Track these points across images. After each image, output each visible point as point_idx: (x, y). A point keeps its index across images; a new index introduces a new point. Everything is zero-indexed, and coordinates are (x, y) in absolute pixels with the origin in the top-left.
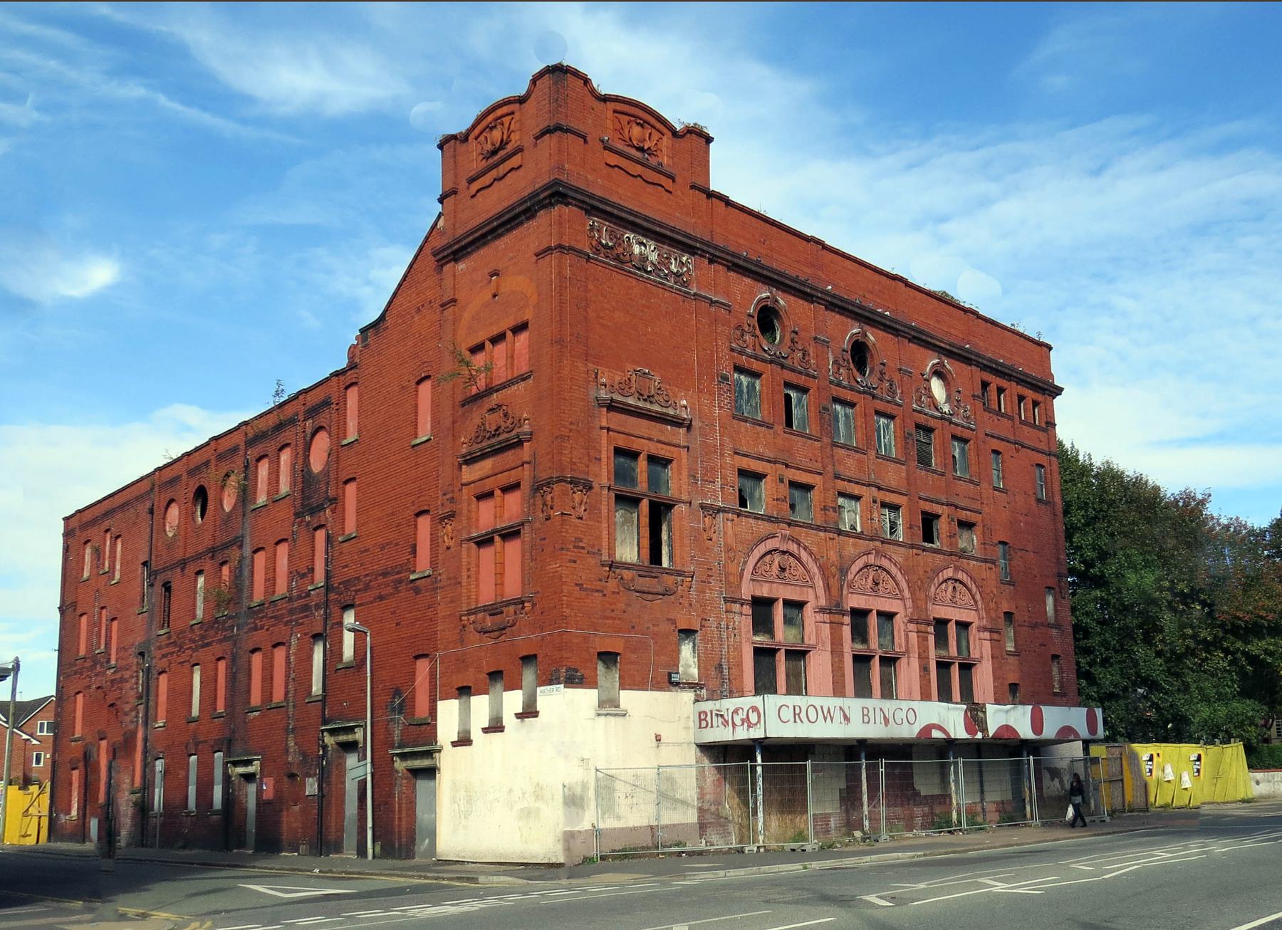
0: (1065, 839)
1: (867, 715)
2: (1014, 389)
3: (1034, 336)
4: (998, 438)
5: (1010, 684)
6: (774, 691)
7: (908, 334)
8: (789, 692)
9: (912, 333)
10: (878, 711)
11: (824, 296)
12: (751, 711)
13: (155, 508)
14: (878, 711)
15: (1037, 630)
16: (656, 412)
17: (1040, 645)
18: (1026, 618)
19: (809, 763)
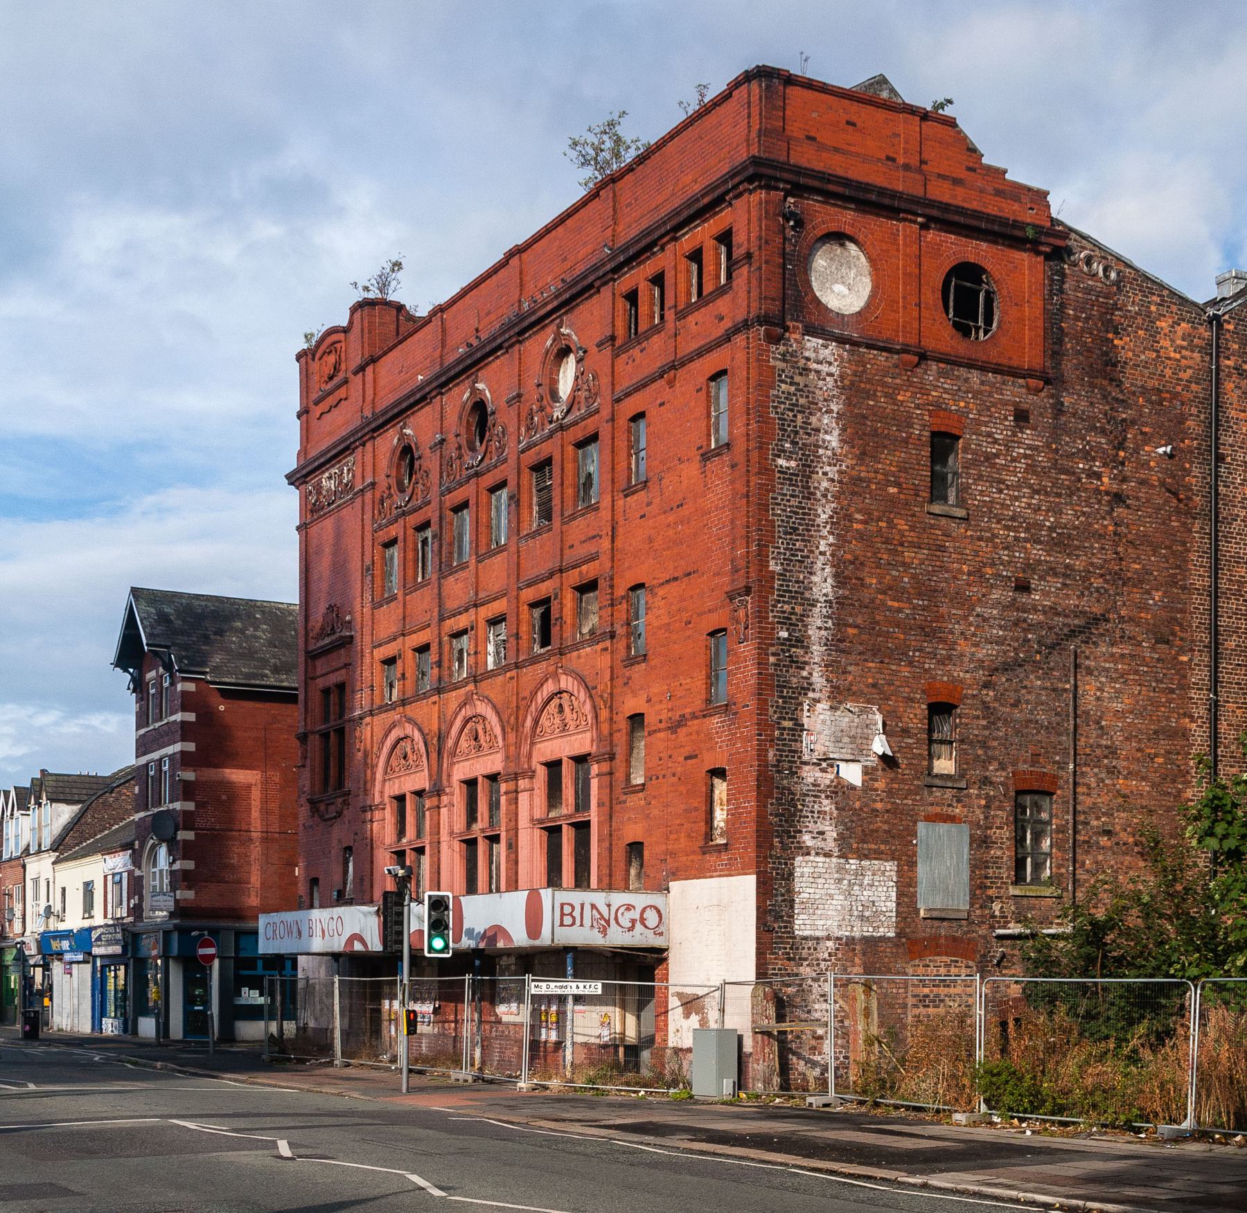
0: (869, 1178)
1: (571, 914)
2: (668, 259)
3: (680, 117)
4: (637, 390)
5: (630, 845)
6: (588, 887)
7: (510, 338)
8: (600, 889)
9: (512, 333)
10: (587, 908)
11: (363, 432)
12: (622, 910)
13: (1072, 670)
14: (587, 908)
15: (682, 732)
16: (330, 643)
17: (686, 758)
18: (663, 717)
19: (467, 977)
